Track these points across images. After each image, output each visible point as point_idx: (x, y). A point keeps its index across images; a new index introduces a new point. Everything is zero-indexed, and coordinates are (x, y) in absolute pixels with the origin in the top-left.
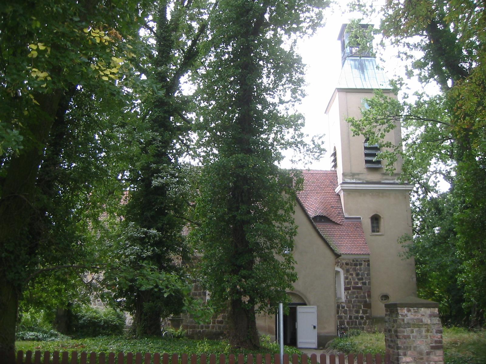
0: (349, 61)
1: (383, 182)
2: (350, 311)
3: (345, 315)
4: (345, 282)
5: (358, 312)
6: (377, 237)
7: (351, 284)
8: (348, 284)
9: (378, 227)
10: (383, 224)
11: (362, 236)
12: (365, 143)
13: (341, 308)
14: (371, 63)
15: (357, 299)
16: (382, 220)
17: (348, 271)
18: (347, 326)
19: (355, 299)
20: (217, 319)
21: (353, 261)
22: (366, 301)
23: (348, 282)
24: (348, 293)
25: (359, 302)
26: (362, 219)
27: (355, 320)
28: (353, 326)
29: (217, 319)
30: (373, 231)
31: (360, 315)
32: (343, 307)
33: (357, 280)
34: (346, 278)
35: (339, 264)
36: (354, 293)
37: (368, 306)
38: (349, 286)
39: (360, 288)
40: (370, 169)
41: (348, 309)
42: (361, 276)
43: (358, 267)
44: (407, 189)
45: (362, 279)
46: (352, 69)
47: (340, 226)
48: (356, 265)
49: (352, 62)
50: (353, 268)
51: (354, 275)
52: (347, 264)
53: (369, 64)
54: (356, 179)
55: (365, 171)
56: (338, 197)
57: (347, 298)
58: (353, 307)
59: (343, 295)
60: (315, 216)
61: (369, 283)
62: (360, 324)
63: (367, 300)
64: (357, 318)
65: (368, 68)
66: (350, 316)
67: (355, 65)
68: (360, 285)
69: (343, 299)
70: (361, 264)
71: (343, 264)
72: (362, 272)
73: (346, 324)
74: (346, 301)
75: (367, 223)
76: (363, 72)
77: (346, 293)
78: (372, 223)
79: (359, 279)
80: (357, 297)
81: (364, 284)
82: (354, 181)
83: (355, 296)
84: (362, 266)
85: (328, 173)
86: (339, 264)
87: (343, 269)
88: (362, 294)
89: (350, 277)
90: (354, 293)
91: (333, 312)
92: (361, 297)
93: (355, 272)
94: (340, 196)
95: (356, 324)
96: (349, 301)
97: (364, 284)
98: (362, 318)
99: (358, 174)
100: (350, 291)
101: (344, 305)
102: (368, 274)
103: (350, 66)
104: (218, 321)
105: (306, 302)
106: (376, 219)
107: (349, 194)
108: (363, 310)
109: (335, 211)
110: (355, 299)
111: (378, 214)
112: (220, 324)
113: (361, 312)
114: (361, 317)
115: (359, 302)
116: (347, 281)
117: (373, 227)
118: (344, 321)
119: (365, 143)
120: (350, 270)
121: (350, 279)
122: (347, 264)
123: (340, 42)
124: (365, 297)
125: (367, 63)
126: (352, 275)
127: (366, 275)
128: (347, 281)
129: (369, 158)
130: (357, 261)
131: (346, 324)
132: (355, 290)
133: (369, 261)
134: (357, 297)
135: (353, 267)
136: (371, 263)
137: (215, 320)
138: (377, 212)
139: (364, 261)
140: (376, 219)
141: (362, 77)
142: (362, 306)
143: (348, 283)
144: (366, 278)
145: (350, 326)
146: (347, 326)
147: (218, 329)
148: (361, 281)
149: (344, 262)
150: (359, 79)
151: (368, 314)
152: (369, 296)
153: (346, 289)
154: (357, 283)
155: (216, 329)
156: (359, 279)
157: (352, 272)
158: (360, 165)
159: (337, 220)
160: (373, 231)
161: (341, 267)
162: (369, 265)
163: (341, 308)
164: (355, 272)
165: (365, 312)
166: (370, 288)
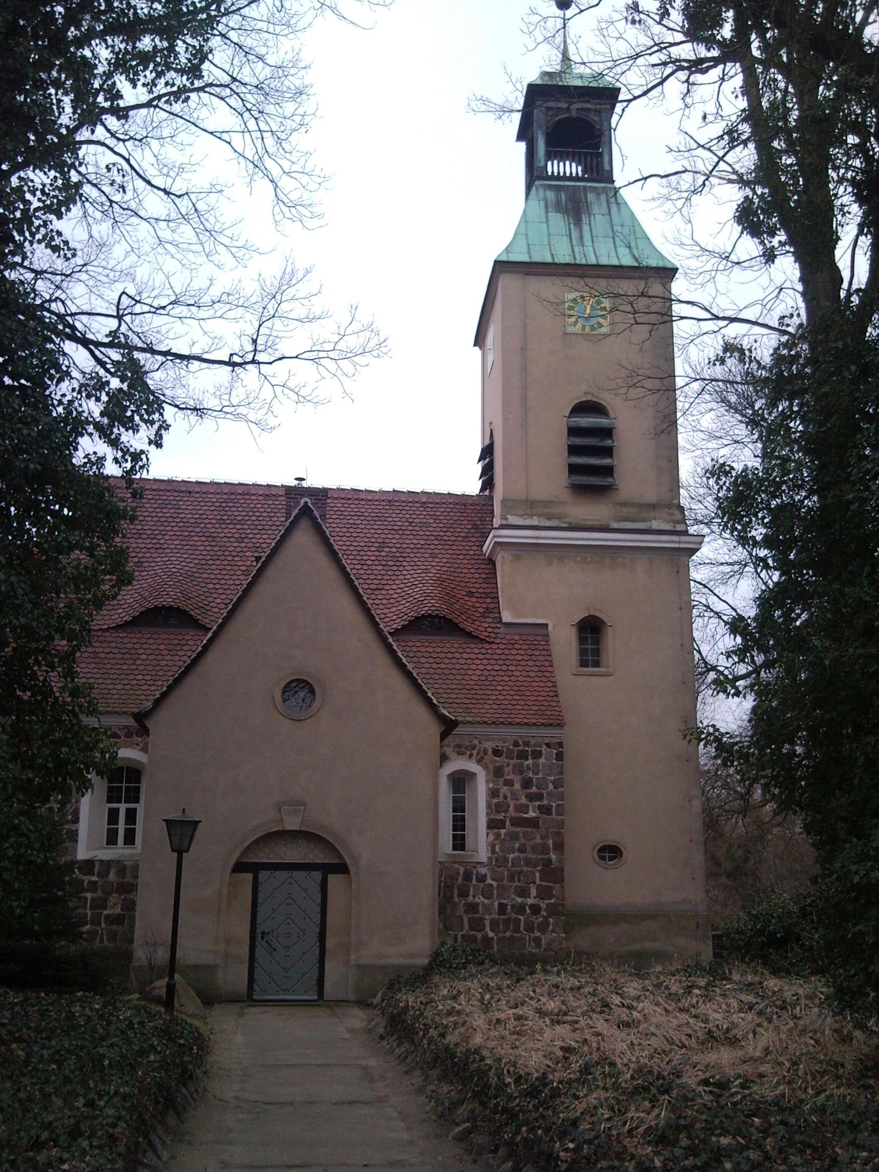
0: (541, 192)
1: (616, 525)
2: (502, 889)
3: (486, 901)
4: (489, 806)
5: (523, 892)
6: (594, 678)
7: (507, 811)
8: (498, 812)
9: (597, 652)
10: (614, 643)
11: (547, 674)
12: (569, 417)
13: (474, 882)
14: (603, 197)
15: (522, 855)
16: (610, 632)
17: (498, 772)
18: (491, 934)
19: (516, 854)
20: (106, 912)
21: (516, 744)
22: (549, 862)
23: (498, 805)
24: (498, 836)
25: (528, 862)
26: (550, 627)
27: (514, 916)
28: (508, 934)
29: (106, 912)
30: (583, 663)
31: (530, 901)
32: (482, 879)
33: (524, 800)
34: (493, 793)
35: (475, 752)
36: (513, 837)
37: (554, 875)
38: (500, 817)
39: (533, 823)
40: (582, 491)
41: (494, 883)
42: (538, 788)
43: (530, 761)
44: (682, 546)
45: (540, 797)
46: (547, 212)
47: (487, 646)
48: (523, 756)
49: (550, 195)
50: (514, 766)
51: (517, 786)
52: (497, 753)
53: (599, 199)
54: (539, 516)
55: (566, 495)
56: (490, 566)
57: (493, 852)
58: (511, 878)
59: (481, 843)
60: (416, 618)
61: (561, 810)
62: (530, 928)
63: (553, 857)
64: (521, 909)
65: (595, 210)
66: (500, 904)
67: (558, 202)
68: (532, 814)
69: (483, 854)
70: (537, 755)
71: (485, 752)
72: (541, 775)
73: (488, 929)
74: (490, 859)
75: (564, 642)
76: (578, 222)
77: (491, 837)
78: (582, 640)
79: (531, 797)
80: (522, 850)
81: (545, 810)
82: (535, 522)
83: (517, 845)
84: (542, 760)
85: (470, 502)
86: (475, 752)
87: (486, 767)
88: (538, 840)
89: (505, 789)
90: (513, 837)
91: (425, 896)
92: (534, 849)
93: (519, 777)
94: (494, 564)
95: (517, 930)
96: (498, 861)
97: (545, 810)
98: (535, 909)
99: (547, 503)
100: (503, 831)
101: (483, 870)
102: (557, 784)
103: (542, 203)
104: (107, 916)
105: (348, 862)
106: (591, 630)
107: (517, 557)
108: (538, 887)
109: (477, 605)
110: (516, 854)
111: (598, 614)
112: (114, 927)
113: (533, 892)
114: (532, 906)
115: (528, 862)
116: (495, 801)
117: (583, 652)
118: (482, 919)
119: (569, 417)
120: (506, 770)
121: (505, 797)
122: (497, 753)
123: (523, 145)
124: (545, 850)
125: (591, 197)
126: (509, 783)
127: (551, 786)
128: (495, 801)
129: (578, 441)
130: (526, 744)
131: (488, 929)
132: (519, 829)
133: (560, 745)
134: (522, 850)
135: (515, 761)
136: (567, 752)
137: (100, 915)
138: (595, 609)
139: (548, 745)
140: (591, 630)
141: (575, 235)
142: (538, 875)
143: (497, 807)
144: (549, 794)
145: (500, 935)
146: (491, 935)
147: (108, 940)
148: (538, 803)
149: (489, 745)
150: (566, 240)
151: (553, 901)
152: (559, 847)
153: (493, 825)
154: (525, 808)
155: (102, 941)
156: (531, 797)
157: (511, 777)
158: (546, 468)
159: (482, 628)
160: (583, 663)
161: (479, 761)
162: (560, 757)
163: (474, 882)
164: (519, 777)
165: (544, 893)
166: (562, 824)
